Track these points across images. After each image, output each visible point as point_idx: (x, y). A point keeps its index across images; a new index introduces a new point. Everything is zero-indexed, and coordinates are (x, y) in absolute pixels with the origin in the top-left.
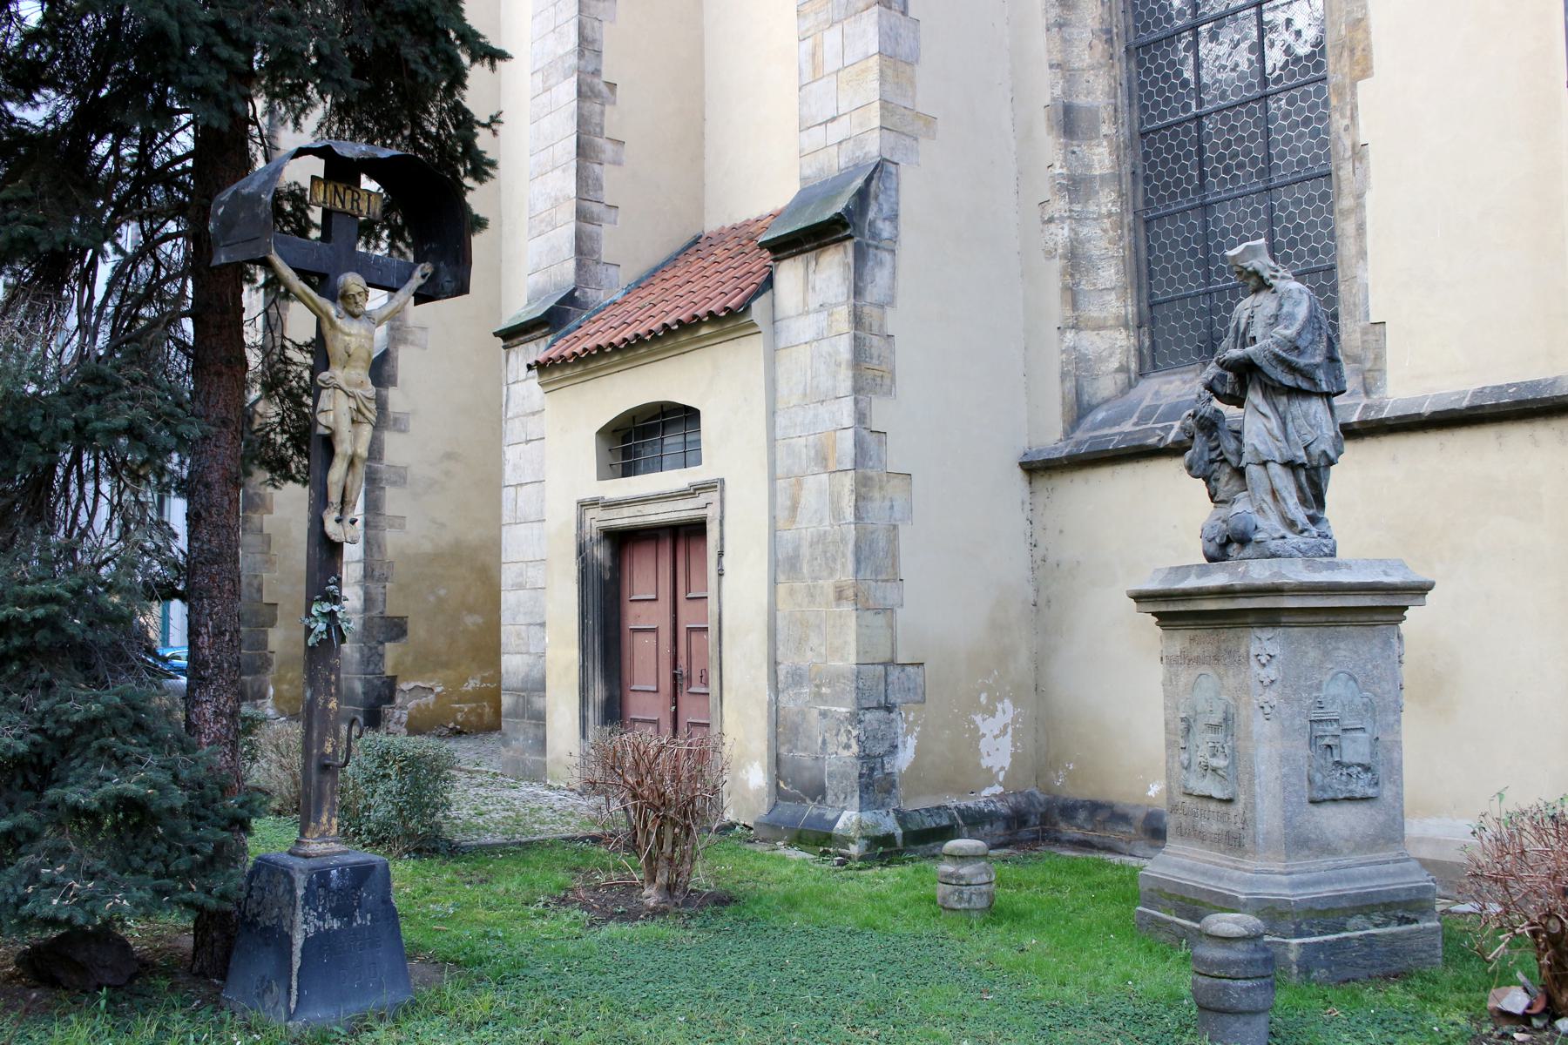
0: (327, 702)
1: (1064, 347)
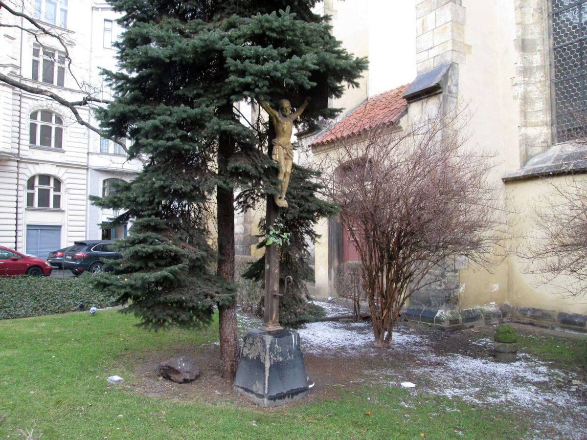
0: (275, 270)
1: (521, 133)
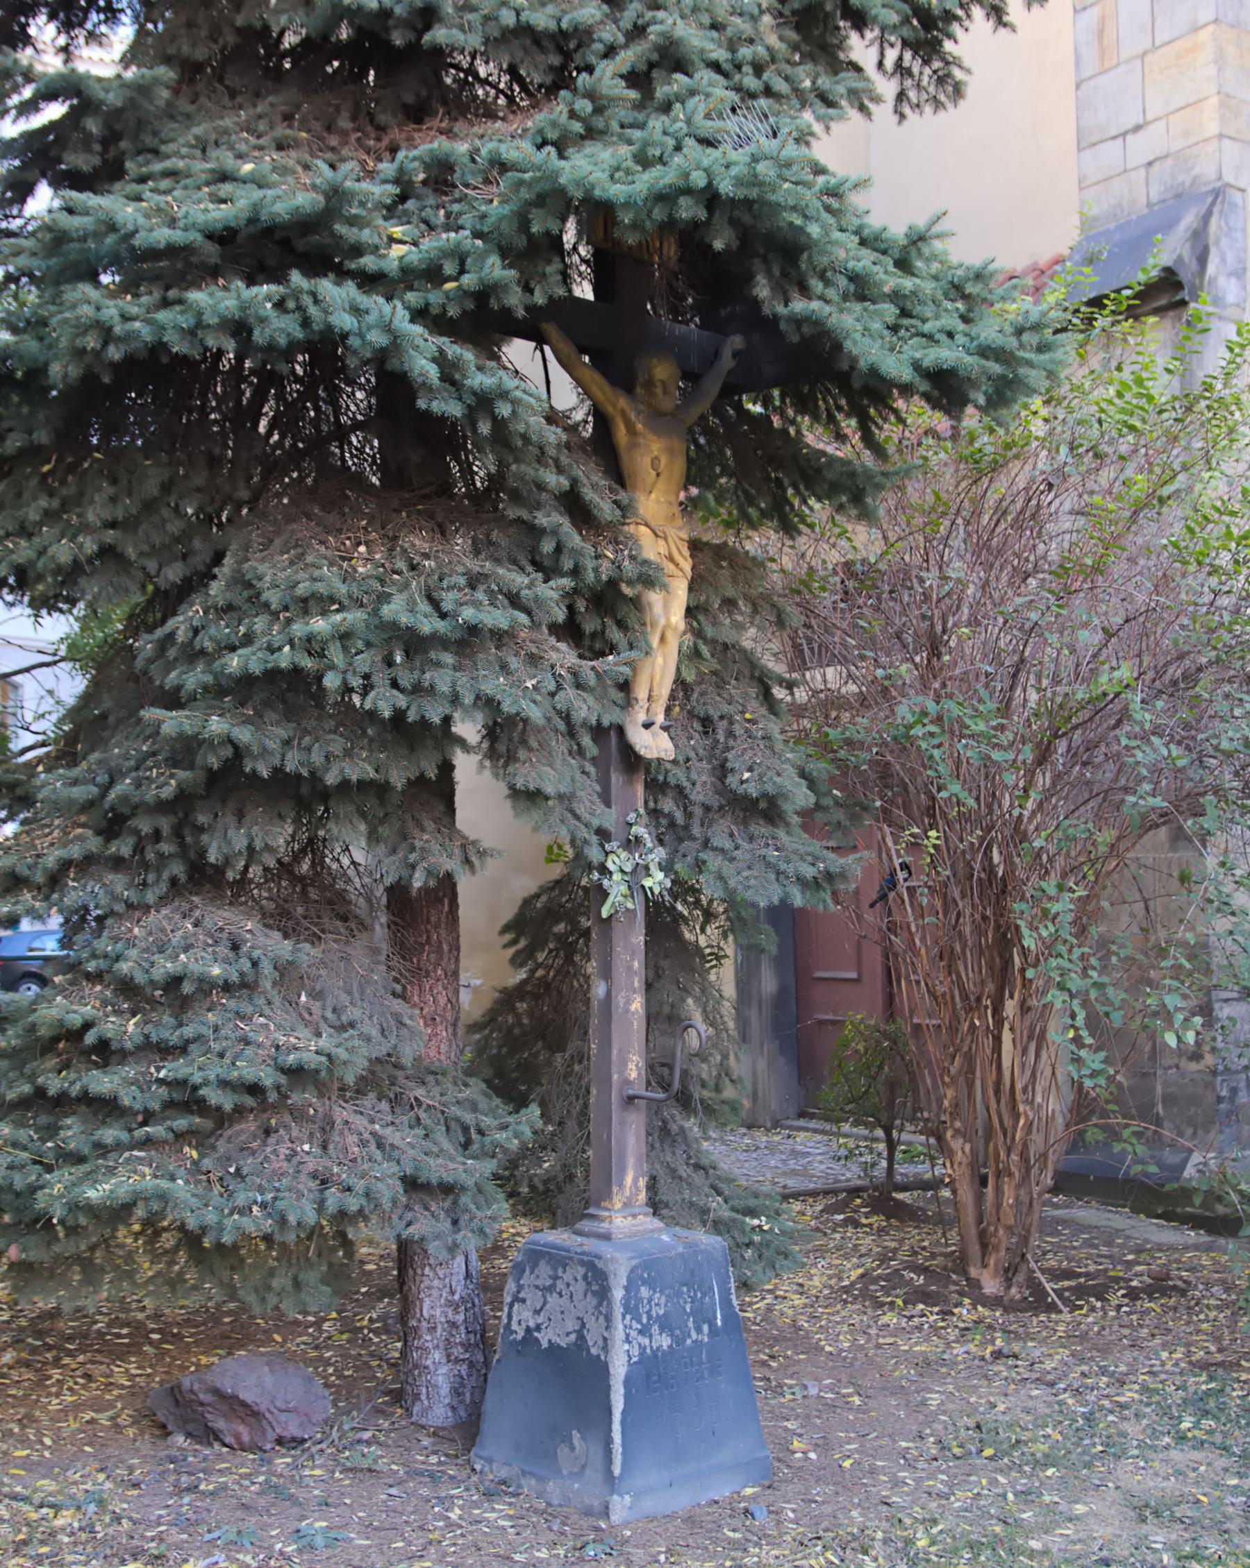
0: (628, 1002)
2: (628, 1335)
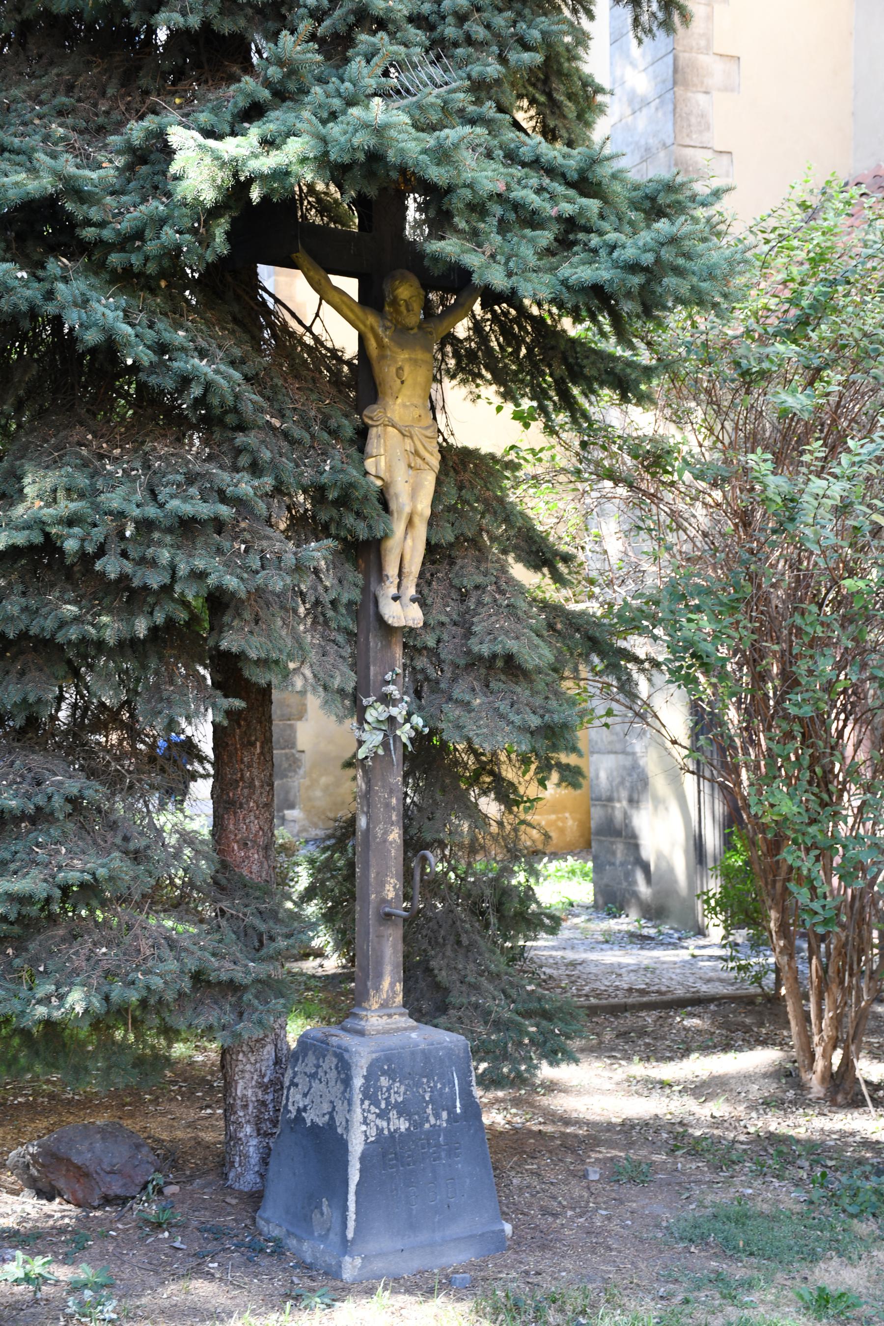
0: (386, 833)
2: (365, 1118)
